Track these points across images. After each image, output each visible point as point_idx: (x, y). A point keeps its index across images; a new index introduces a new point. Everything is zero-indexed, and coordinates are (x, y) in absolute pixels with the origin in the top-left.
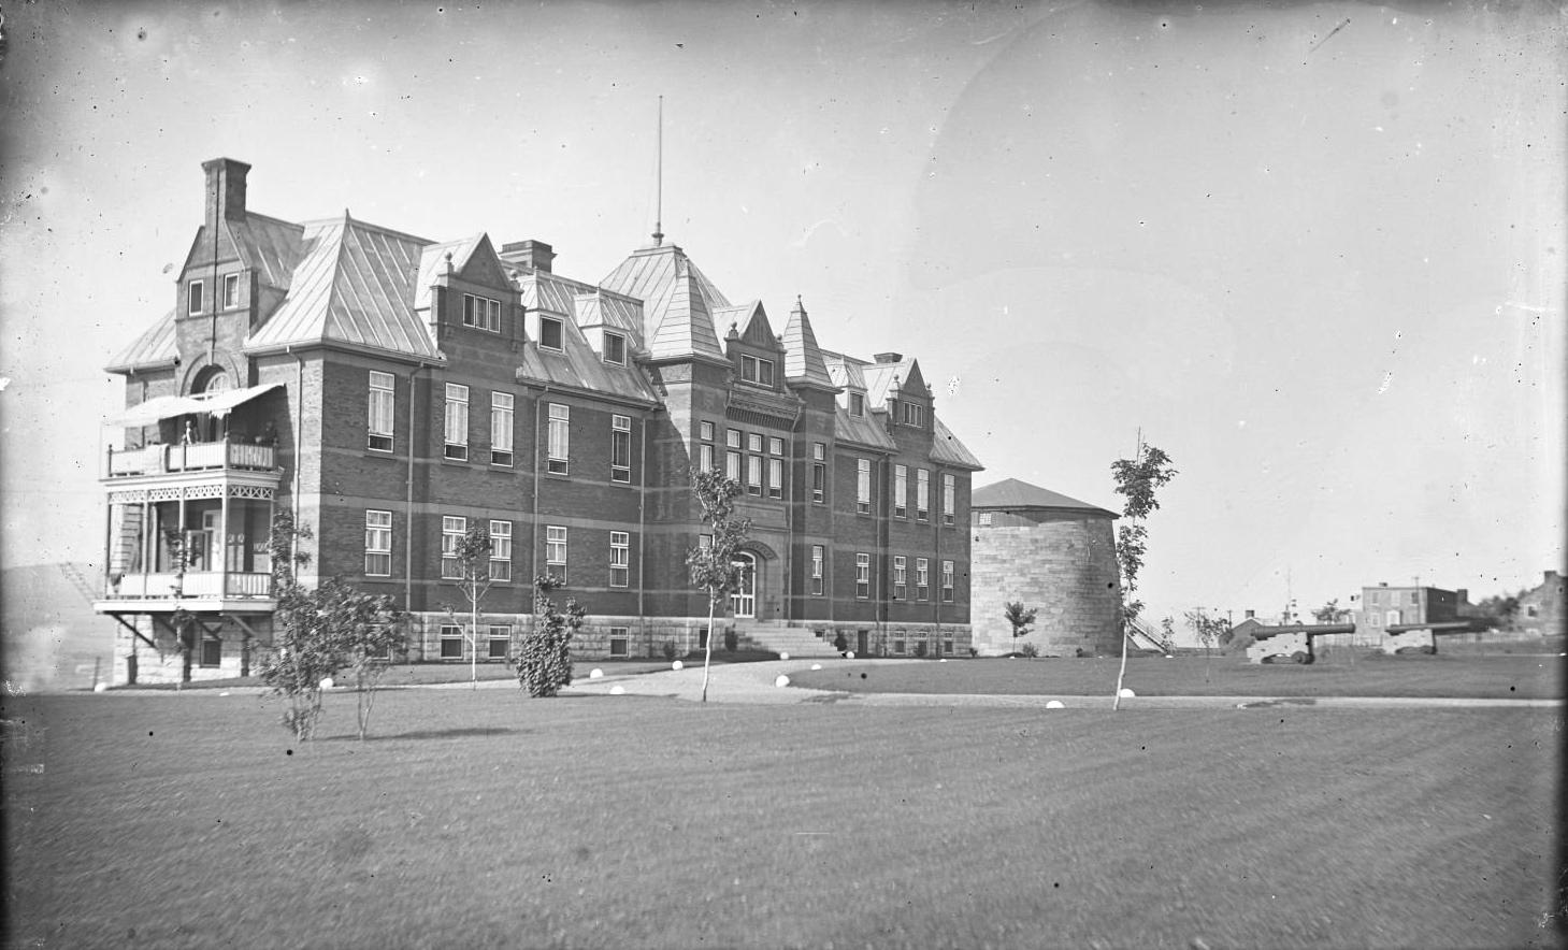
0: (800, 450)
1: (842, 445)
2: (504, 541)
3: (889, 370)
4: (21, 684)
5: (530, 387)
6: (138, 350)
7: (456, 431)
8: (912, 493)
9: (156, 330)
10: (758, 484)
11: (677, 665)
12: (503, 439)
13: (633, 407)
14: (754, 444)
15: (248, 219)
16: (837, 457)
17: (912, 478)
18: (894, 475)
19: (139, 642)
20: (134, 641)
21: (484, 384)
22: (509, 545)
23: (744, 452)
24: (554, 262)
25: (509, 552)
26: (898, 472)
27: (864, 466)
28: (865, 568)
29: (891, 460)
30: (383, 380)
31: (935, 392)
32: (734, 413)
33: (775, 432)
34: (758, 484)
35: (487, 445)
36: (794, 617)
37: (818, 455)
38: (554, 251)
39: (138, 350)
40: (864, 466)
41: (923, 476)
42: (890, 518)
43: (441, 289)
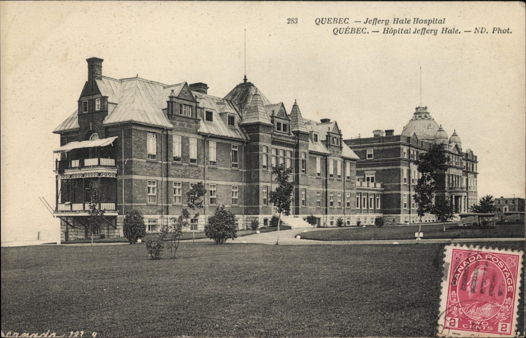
0: (297, 154)
1: (311, 153)
2: (179, 189)
3: (326, 126)
4: (2, 246)
5: (203, 136)
6: (65, 125)
7: (177, 151)
8: (335, 169)
9: (70, 118)
10: (196, 158)
11: (258, 232)
12: (193, 154)
13: (239, 141)
14: (281, 154)
15: (103, 79)
16: (310, 157)
17: (335, 162)
18: (109, 124)
19: (68, 226)
20: (67, 226)
21: (186, 135)
22: (156, 189)
23: (278, 156)
24: (208, 90)
25: (156, 192)
26: (330, 162)
27: (318, 160)
28: (179, 189)
29: (328, 158)
30: (178, 138)
31: (94, 56)
32: (274, 142)
33: (289, 149)
34: (196, 158)
35: (188, 157)
36: (296, 214)
37: (303, 157)
38: (208, 86)
39: (65, 125)
40: (318, 160)
41: (339, 164)
42: (328, 178)
43: (168, 102)
